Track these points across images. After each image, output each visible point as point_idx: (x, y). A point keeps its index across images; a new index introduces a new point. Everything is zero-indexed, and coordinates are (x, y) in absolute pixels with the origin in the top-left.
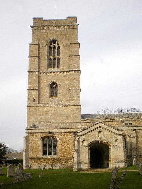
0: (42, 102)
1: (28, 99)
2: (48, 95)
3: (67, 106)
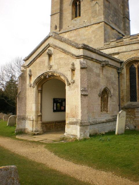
0: (65, 27)
1: (51, 27)
2: (70, 18)
3: (87, 26)
